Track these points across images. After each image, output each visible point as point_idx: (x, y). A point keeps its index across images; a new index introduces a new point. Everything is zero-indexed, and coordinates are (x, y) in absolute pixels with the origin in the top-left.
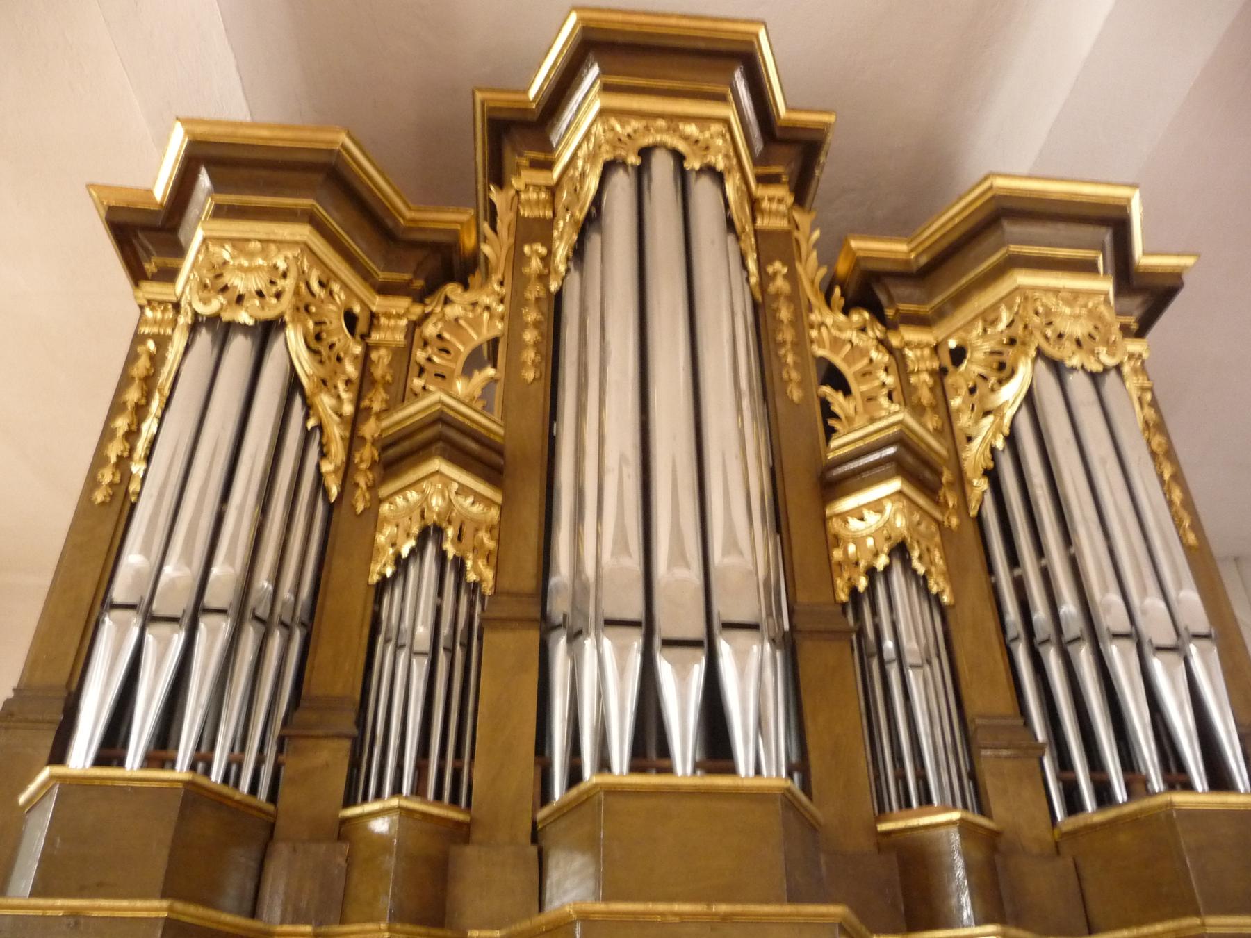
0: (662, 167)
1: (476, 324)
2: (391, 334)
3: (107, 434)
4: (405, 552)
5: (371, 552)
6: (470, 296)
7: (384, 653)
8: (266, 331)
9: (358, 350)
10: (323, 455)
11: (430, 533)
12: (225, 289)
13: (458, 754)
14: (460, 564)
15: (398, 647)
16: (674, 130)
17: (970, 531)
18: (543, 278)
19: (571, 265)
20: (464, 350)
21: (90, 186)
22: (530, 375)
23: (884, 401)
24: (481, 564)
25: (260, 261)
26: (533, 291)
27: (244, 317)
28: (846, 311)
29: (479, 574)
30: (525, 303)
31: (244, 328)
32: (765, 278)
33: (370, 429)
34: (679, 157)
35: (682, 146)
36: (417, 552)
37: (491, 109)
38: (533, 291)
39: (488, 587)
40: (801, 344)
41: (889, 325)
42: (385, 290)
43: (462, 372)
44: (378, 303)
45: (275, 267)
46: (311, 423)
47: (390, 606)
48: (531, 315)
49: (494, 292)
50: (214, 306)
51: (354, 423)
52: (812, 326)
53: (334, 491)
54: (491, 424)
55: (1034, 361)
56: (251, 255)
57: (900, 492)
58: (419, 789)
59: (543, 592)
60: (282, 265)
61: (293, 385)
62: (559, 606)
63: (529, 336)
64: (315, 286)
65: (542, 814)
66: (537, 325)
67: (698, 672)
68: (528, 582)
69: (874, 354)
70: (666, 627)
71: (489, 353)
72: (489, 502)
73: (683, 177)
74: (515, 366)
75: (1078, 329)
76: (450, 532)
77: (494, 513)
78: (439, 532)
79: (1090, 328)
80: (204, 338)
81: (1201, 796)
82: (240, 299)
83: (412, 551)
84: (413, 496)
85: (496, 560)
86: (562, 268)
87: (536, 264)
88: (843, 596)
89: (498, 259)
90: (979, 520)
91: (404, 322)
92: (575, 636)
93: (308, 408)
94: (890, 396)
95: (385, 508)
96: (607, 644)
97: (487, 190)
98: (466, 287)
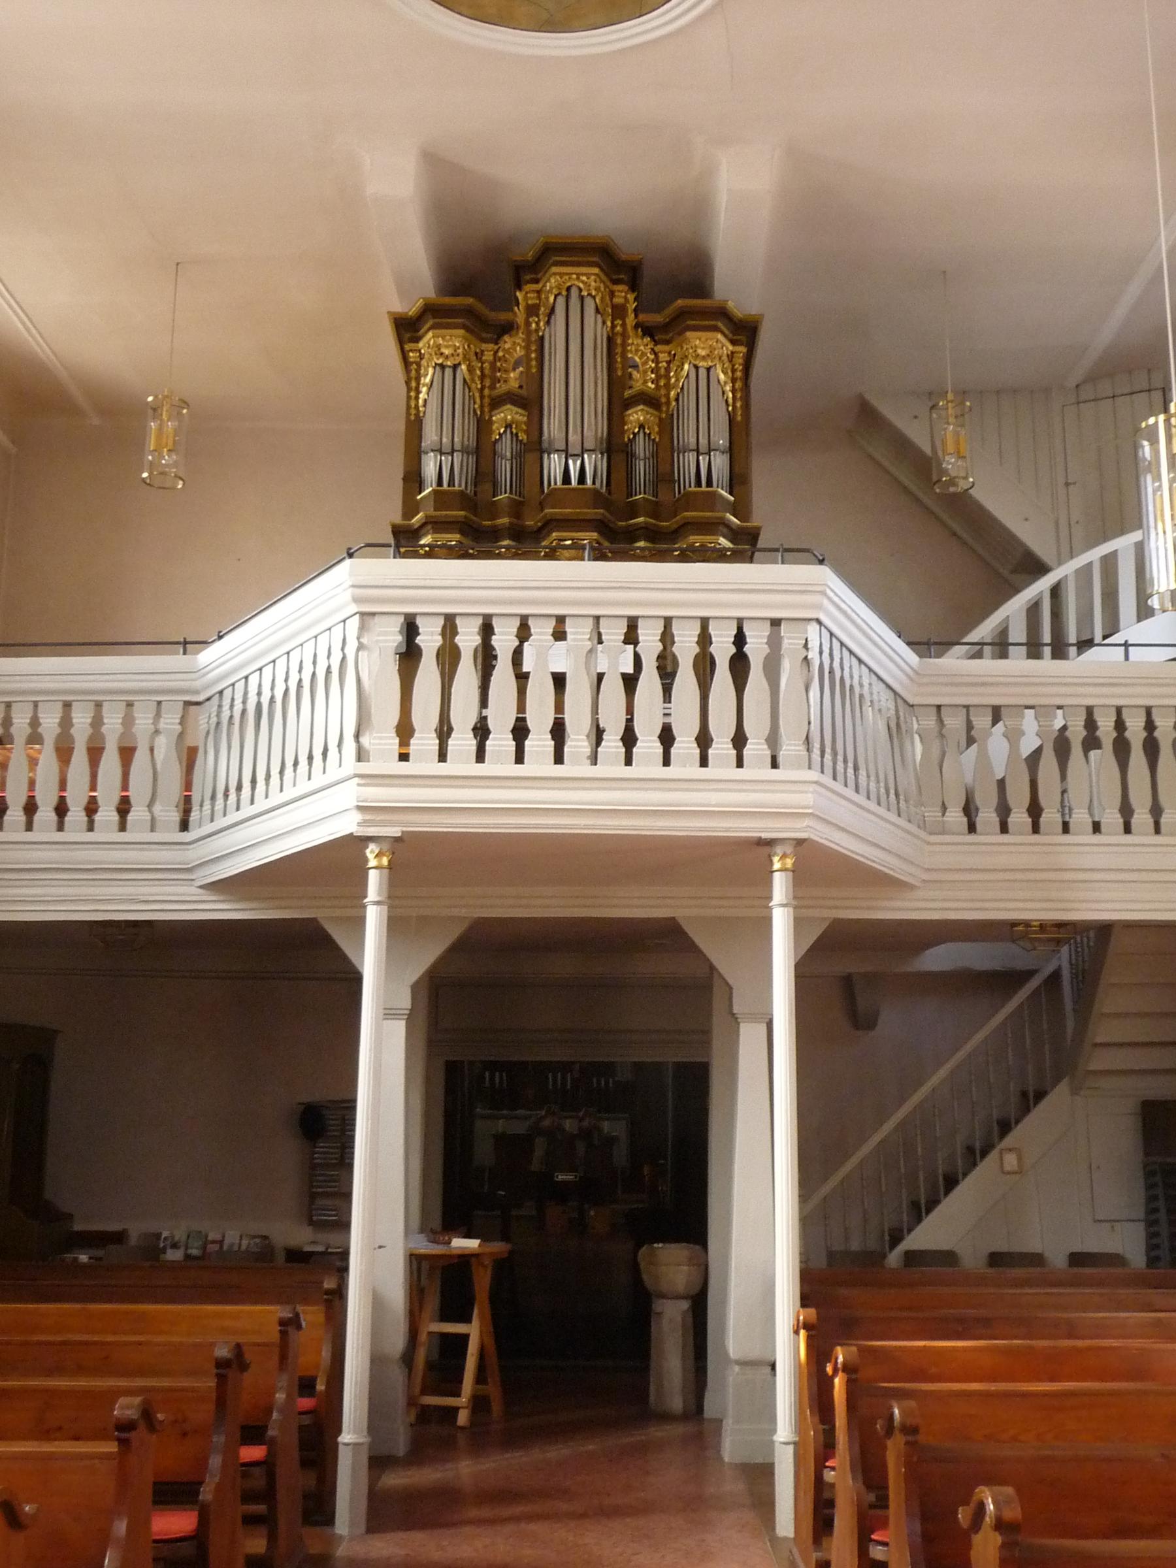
0: (574, 293)
2: (488, 356)
3: (409, 398)
6: (513, 339)
7: (498, 460)
8: (455, 367)
9: (480, 365)
10: (475, 403)
11: (508, 426)
12: (442, 354)
13: (520, 487)
15: (502, 459)
16: (578, 278)
18: (537, 331)
20: (513, 360)
21: (388, 312)
22: (534, 370)
23: (649, 373)
25: (450, 343)
26: (534, 338)
27: (449, 363)
30: (531, 360)
31: (450, 367)
32: (613, 326)
33: (486, 392)
34: (580, 290)
35: (581, 285)
39: (525, 441)
41: (656, 343)
44: (484, 346)
45: (455, 345)
46: (471, 394)
47: (498, 447)
49: (520, 338)
50: (440, 361)
52: (629, 345)
56: (448, 341)
58: (511, 493)
59: (540, 442)
60: (457, 344)
61: (465, 380)
62: (545, 445)
65: (542, 497)
66: (536, 351)
67: (579, 462)
69: (649, 355)
72: (524, 416)
73: (582, 298)
74: (528, 367)
75: (702, 353)
76: (514, 426)
77: (525, 418)
81: (693, 489)
83: (504, 432)
84: (502, 415)
85: (527, 432)
87: (534, 326)
88: (626, 439)
90: (673, 415)
91: (492, 353)
92: (549, 454)
93: (469, 389)
95: (494, 418)
96: (691, 454)
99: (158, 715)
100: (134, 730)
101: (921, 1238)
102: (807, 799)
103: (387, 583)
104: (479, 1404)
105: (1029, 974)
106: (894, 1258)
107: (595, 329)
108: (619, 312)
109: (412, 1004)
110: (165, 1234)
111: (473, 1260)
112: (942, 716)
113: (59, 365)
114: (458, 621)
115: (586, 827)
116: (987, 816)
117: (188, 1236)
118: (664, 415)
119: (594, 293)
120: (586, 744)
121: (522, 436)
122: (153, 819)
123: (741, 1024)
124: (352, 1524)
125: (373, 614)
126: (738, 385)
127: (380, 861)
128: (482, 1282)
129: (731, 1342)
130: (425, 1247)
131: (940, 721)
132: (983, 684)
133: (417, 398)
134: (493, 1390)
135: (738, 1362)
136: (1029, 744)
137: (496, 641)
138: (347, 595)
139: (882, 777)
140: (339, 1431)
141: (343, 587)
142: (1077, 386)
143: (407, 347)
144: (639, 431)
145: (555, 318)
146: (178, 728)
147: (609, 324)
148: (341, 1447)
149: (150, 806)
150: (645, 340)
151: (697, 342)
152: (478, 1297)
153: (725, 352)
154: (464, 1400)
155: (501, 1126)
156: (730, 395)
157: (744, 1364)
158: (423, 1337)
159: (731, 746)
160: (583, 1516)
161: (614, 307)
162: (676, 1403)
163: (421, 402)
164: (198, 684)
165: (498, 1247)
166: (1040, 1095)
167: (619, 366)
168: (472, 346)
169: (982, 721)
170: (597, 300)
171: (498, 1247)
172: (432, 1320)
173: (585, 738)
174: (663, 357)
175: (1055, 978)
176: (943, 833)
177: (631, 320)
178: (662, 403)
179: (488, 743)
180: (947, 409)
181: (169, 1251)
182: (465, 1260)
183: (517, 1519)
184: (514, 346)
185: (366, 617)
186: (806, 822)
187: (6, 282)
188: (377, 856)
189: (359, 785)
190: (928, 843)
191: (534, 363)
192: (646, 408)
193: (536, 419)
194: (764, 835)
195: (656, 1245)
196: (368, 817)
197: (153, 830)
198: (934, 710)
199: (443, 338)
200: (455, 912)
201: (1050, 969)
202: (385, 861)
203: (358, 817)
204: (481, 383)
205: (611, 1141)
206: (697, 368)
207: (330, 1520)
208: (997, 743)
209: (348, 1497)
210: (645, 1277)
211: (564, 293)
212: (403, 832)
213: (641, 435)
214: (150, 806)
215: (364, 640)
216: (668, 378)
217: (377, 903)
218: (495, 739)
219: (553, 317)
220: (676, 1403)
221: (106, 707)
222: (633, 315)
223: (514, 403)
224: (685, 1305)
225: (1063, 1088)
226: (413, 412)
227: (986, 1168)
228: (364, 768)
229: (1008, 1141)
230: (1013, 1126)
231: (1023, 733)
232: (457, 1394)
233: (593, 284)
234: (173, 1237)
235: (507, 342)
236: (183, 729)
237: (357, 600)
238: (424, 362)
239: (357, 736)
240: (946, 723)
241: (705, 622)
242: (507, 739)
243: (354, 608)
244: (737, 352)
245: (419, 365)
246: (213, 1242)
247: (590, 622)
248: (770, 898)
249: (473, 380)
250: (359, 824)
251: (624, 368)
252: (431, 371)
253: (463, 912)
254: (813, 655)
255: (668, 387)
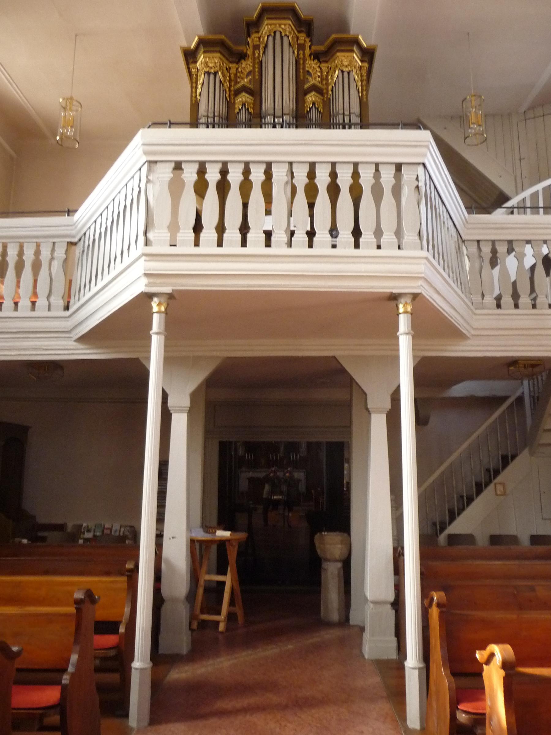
0: (278, 34)
1: (247, 68)
2: (233, 71)
3: (192, 92)
4: (240, 108)
5: (235, 108)
8: (215, 74)
9: (229, 75)
10: (226, 93)
14: (248, 109)
17: (328, 102)
18: (258, 57)
19: (263, 55)
20: (246, 73)
22: (257, 77)
24: (251, 109)
26: (257, 61)
28: (313, 60)
29: (251, 111)
32: (298, 54)
33: (232, 89)
34: (281, 32)
35: (281, 30)
36: (242, 108)
37: (247, 21)
38: (257, 61)
40: (304, 68)
42: (231, 62)
43: (515, 307)
44: (231, 65)
47: (238, 117)
48: (257, 66)
51: (230, 88)
53: (228, 99)
54: (251, 86)
55: (339, 70)
57: (314, 95)
61: (221, 81)
63: (257, 70)
64: (221, 64)
68: (258, 111)
70: (276, 114)
71: (249, 73)
73: (282, 38)
75: (346, 63)
76: (246, 105)
77: (253, 102)
78: (245, 105)
79: (349, 63)
80: (206, 75)
82: (211, 68)
83: (241, 108)
85: (254, 109)
86: (262, 56)
87: (257, 55)
89: (250, 54)
90: (330, 99)
93: (223, 86)
94: (319, 77)
97: (247, 38)
98: (245, 60)
99: (53, 250)
100: (40, 257)
101: (457, 528)
102: (421, 268)
103: (164, 142)
104: (231, 617)
105: (504, 399)
106: (442, 538)
107: (289, 57)
108: (301, 47)
109: (191, 403)
110: (85, 525)
111: (227, 543)
112: (480, 246)
113: (33, 111)
114: (207, 166)
115: (285, 286)
116: (507, 300)
117: (95, 527)
118: (325, 99)
119: (288, 34)
120: (285, 235)
121: (251, 110)
122: (50, 305)
123: (372, 415)
124: (139, 721)
125: (156, 162)
126: (364, 83)
127: (160, 308)
128: (232, 555)
129: (368, 592)
130: (201, 535)
131: (479, 249)
132: (503, 228)
133: (196, 92)
134: (239, 611)
135: (373, 602)
136: (529, 261)
137: (230, 177)
138: (140, 152)
139: (454, 270)
140: (132, 659)
141: (138, 147)
142: (525, 112)
143: (191, 67)
144: (312, 107)
145: (268, 49)
146: (65, 256)
147: (296, 52)
148: (133, 671)
149: (48, 297)
150: (315, 61)
151: (343, 58)
152: (230, 562)
153: (358, 65)
154: (222, 617)
155: (251, 474)
156: (360, 88)
157: (375, 603)
158: (202, 583)
159: (373, 237)
160: (285, 707)
161: (298, 45)
162: (335, 617)
163: (198, 93)
164: (73, 232)
165: (242, 536)
166: (514, 457)
167: (302, 74)
168: (224, 64)
169: (502, 249)
170: (290, 38)
171: (242, 536)
172: (209, 572)
173: (284, 232)
174: (325, 70)
175: (520, 400)
176: (483, 308)
177: (307, 51)
178: (324, 93)
179: (225, 235)
180: (471, 101)
181: (86, 533)
182: (222, 544)
183: (245, 710)
184: (246, 65)
185: (152, 163)
186: (420, 282)
187: (3, 64)
188: (158, 305)
189: (145, 261)
190: (475, 314)
191: (257, 74)
192: (316, 94)
193: (258, 102)
194: (394, 291)
195: (323, 533)
196: (152, 280)
197: (49, 309)
198: (476, 243)
199: (209, 58)
200: (214, 354)
201: (518, 394)
202: (163, 309)
203: (145, 280)
204: (230, 84)
205: (299, 481)
206: (343, 72)
207: (126, 715)
208: (511, 262)
209: (136, 703)
210: (318, 551)
211: (272, 34)
212: (173, 290)
213: (314, 107)
214: (48, 297)
215: (151, 178)
216: (327, 79)
217: (158, 333)
218: (228, 233)
219: (267, 49)
220: (335, 617)
221: (25, 245)
222: (309, 49)
223: (247, 92)
224: (339, 565)
225: (526, 452)
226: (194, 99)
227: (488, 492)
228: (149, 250)
229: (499, 479)
230: (501, 472)
231: (525, 255)
232: (219, 613)
233: (288, 29)
234: (88, 526)
235: (244, 64)
236: (66, 257)
237: (146, 153)
238: (199, 74)
239: (145, 233)
240: (482, 250)
241: (356, 165)
242: (236, 233)
243: (144, 159)
244: (363, 67)
245: (197, 76)
246: (107, 529)
247: (287, 166)
248: (397, 330)
249: (225, 81)
250: (146, 285)
251: (304, 76)
252: (203, 76)
253: (218, 354)
254: (421, 184)
255: (327, 84)
